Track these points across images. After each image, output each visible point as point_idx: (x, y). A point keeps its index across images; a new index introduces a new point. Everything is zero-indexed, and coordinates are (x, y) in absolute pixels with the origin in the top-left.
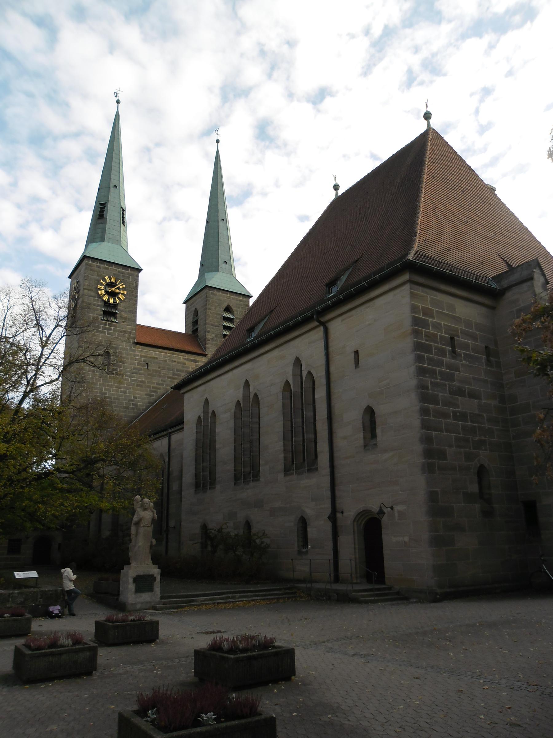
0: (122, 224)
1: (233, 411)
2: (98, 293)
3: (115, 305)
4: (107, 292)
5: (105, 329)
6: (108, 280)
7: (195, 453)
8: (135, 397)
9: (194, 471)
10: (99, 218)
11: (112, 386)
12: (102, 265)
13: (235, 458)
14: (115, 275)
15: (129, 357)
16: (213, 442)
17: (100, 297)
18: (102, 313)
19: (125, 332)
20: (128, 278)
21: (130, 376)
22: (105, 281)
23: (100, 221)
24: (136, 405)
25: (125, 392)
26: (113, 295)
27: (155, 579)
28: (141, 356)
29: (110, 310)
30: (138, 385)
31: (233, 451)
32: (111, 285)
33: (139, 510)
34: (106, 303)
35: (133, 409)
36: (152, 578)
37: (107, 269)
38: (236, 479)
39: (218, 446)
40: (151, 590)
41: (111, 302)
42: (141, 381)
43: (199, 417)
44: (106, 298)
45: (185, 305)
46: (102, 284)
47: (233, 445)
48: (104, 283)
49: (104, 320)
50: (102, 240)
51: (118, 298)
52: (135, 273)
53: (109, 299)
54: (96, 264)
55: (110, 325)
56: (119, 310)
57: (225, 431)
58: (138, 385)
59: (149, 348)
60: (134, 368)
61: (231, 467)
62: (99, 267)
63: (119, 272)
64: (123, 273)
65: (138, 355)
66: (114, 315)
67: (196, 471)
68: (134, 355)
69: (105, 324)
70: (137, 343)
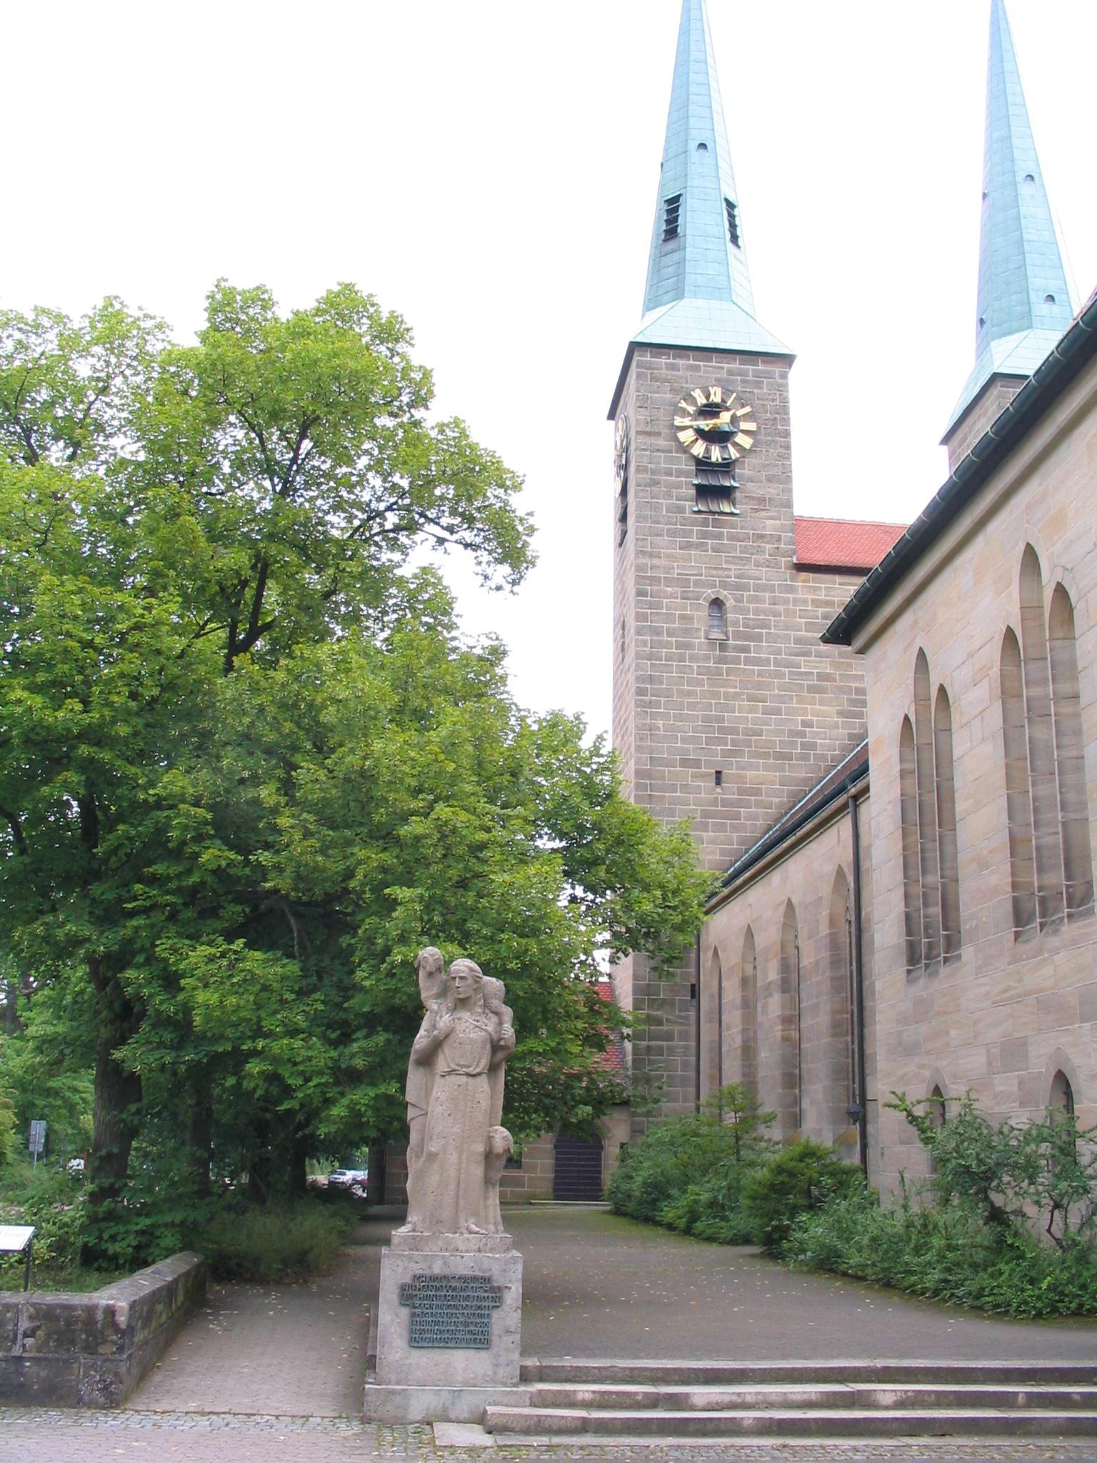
0: (730, 245)
1: (996, 671)
2: (677, 440)
3: (726, 467)
4: (701, 433)
5: (705, 535)
6: (701, 400)
7: (900, 845)
8: (806, 724)
9: (900, 908)
10: (665, 241)
11: (736, 696)
12: (680, 362)
13: (1014, 843)
14: (719, 382)
15: (780, 608)
16: (945, 797)
17: (684, 449)
18: (693, 492)
19: (761, 537)
20: (759, 385)
21: (788, 665)
22: (693, 401)
23: (672, 245)
24: (813, 746)
25: (777, 712)
26: (718, 437)
27: (495, 1294)
28: (816, 603)
29: (714, 482)
30: (812, 689)
31: (1005, 816)
32: (710, 410)
33: (432, 1005)
34: (703, 465)
35: (805, 757)
36: (484, 1291)
37: (697, 368)
38: (1020, 917)
39: (960, 807)
40: (480, 1340)
41: (713, 459)
42: (821, 677)
43: (906, 718)
44: (699, 449)
45: (945, 448)
46: (684, 413)
47: (1004, 792)
48: (691, 409)
49: (699, 512)
50: (678, 293)
51: (736, 445)
52: (776, 369)
53: (707, 450)
54: (663, 360)
55: (716, 524)
56: (742, 478)
57: (977, 755)
58: (812, 689)
59: (838, 578)
60: (798, 641)
61: (999, 876)
62: (673, 367)
63: (730, 372)
64: (743, 374)
65: (805, 602)
66: (725, 493)
67: (907, 905)
68: (795, 600)
69: (705, 523)
70: (802, 567)
